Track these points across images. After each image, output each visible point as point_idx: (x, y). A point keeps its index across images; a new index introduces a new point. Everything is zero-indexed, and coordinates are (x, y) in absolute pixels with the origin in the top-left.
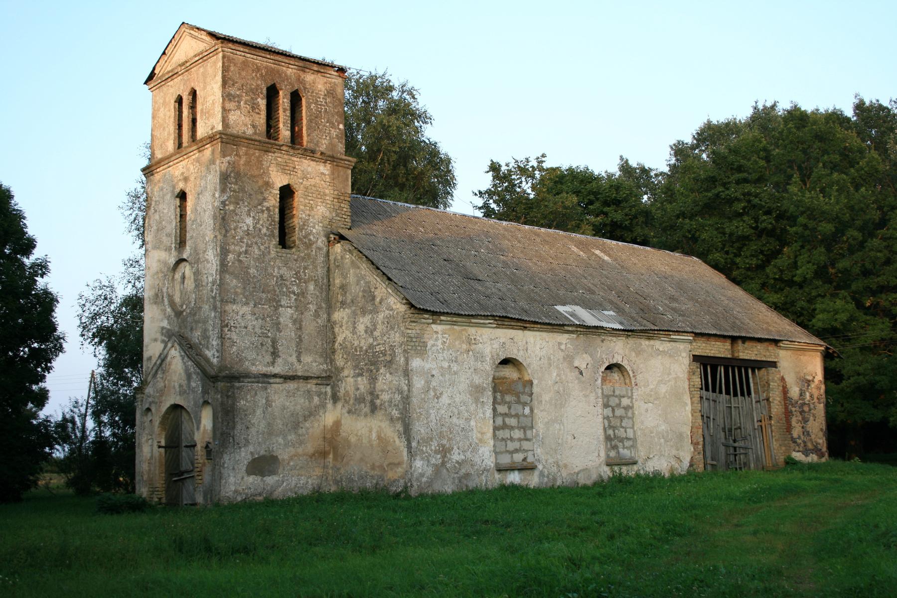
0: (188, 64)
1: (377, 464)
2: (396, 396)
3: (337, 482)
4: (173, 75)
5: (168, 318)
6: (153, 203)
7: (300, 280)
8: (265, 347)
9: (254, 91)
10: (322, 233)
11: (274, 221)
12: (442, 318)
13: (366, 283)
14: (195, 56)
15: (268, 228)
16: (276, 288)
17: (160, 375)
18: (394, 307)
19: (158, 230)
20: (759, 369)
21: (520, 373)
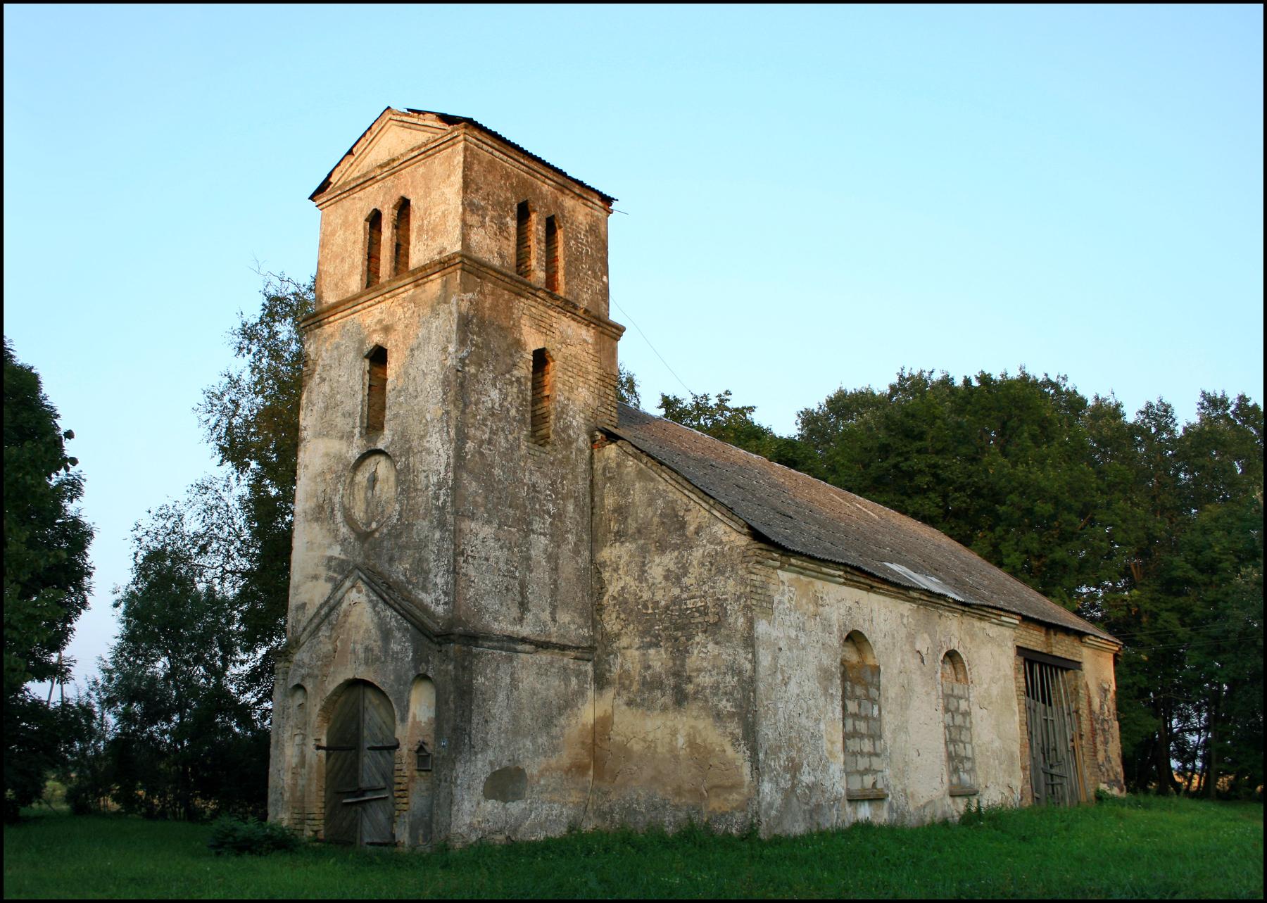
0: (396, 164)
1: (687, 787)
2: (728, 678)
3: (602, 815)
4: (367, 180)
5: (343, 542)
6: (319, 369)
7: (556, 495)
8: (510, 593)
9: (502, 205)
10: (584, 428)
11: (524, 399)
12: (793, 561)
13: (667, 502)
14: (412, 150)
15: (518, 410)
16: (527, 503)
17: (324, 632)
18: (725, 539)
19: (326, 408)
20: (1067, 670)
21: (860, 656)
